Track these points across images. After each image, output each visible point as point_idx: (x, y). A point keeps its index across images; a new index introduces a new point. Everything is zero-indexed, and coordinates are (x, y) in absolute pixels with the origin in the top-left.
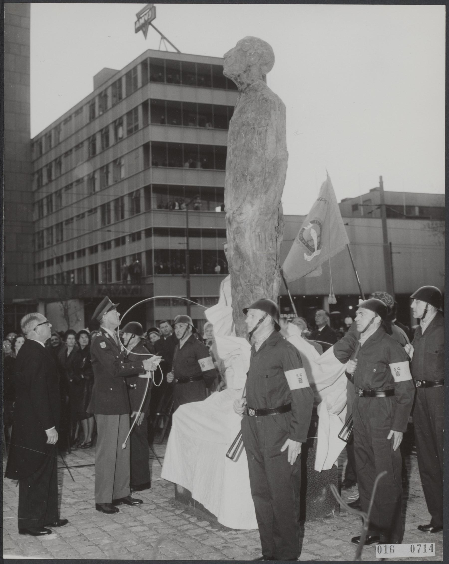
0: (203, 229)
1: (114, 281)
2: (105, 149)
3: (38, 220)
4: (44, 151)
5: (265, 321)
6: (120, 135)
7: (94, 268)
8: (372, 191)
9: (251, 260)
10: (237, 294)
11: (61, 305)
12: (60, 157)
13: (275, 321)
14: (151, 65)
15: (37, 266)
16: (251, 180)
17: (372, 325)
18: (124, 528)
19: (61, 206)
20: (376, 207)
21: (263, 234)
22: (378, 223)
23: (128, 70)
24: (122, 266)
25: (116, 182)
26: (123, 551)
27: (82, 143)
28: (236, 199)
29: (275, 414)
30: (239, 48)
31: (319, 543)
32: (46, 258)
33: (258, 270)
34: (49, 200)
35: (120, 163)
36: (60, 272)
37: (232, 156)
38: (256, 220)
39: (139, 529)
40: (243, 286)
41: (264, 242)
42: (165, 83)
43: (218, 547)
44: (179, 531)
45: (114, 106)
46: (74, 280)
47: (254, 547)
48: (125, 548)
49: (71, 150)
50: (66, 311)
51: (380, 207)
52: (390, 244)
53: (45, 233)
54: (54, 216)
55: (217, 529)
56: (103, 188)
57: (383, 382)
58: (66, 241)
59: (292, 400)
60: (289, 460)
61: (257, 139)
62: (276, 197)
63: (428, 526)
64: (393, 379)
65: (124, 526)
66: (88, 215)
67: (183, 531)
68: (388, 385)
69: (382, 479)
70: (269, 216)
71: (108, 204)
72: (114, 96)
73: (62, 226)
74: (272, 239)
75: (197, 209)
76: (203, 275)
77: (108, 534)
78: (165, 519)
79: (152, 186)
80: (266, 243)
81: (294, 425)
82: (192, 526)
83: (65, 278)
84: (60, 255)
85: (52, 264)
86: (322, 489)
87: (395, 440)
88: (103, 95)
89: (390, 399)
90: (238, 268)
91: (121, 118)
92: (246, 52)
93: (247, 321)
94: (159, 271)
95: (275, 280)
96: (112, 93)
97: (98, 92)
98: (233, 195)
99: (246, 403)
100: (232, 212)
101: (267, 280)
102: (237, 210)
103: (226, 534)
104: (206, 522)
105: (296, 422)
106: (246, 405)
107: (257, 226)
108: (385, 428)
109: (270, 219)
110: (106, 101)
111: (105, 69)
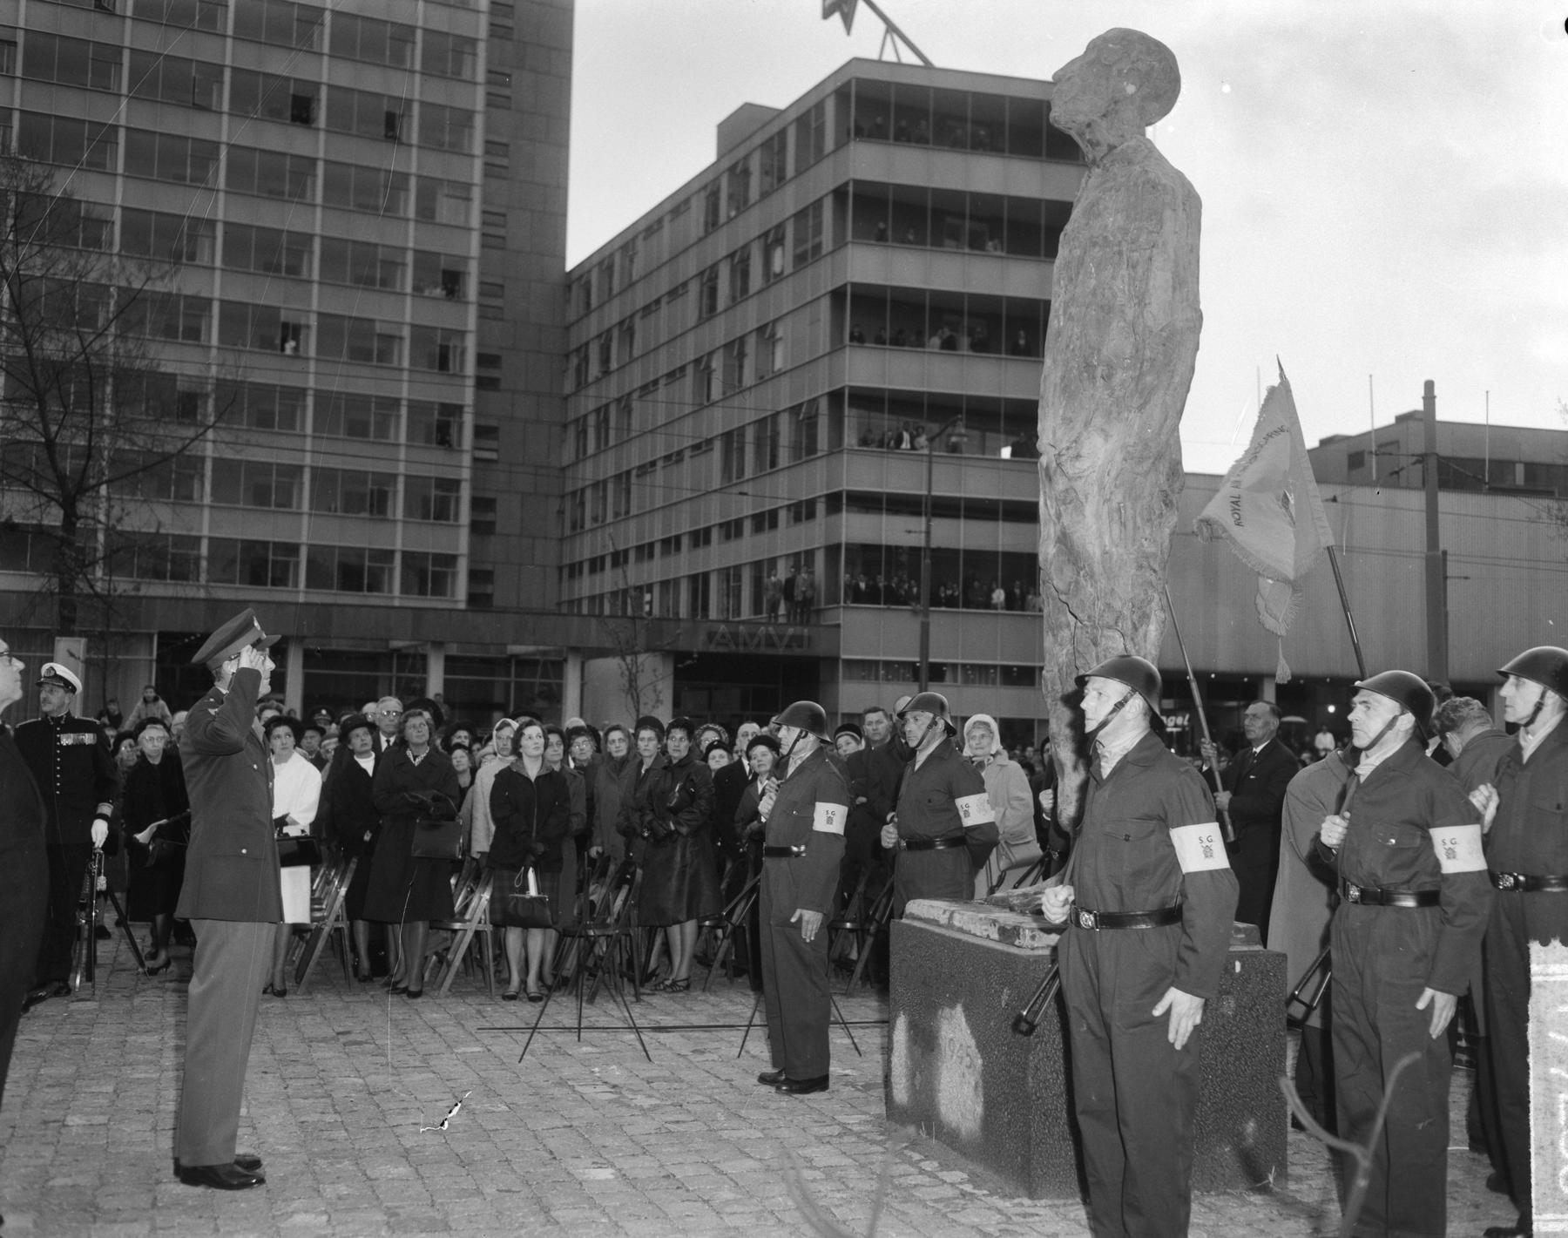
1: (746, 613)
4: (594, 303)
5: (1127, 707)
6: (777, 268)
7: (699, 583)
8: (1401, 419)
9: (1098, 569)
10: (1058, 648)
12: (632, 316)
13: (1151, 709)
14: (858, 97)
16: (1107, 378)
17: (1389, 735)
19: (629, 430)
20: (1415, 459)
21: (1128, 504)
22: (1417, 499)
23: (803, 110)
24: (766, 580)
25: (762, 380)
26: (766, 1220)
27: (685, 285)
29: (1144, 926)
30: (1093, 56)
32: (587, 555)
35: (773, 335)
38: (1113, 474)
41: (1130, 525)
42: (891, 141)
43: (991, 1230)
45: (765, 195)
46: (651, 608)
48: (772, 1212)
49: (658, 301)
50: (632, 680)
51: (1422, 459)
52: (1445, 553)
53: (588, 494)
54: (611, 455)
55: (985, 1192)
57: (1412, 871)
60: (1171, 1037)
62: (1166, 420)
64: (1437, 865)
66: (692, 457)
67: (906, 1189)
70: (1147, 465)
71: (741, 430)
72: (766, 172)
73: (628, 479)
75: (954, 449)
78: (863, 1159)
80: (1136, 528)
81: (1186, 955)
82: (926, 1180)
85: (603, 568)
87: (1437, 1012)
88: (739, 170)
91: (780, 227)
94: (857, 596)
95: (1153, 618)
96: (762, 165)
97: (726, 164)
98: (1061, 412)
99: (1072, 898)
100: (1053, 452)
101: (1134, 617)
102: (1068, 448)
103: (1008, 1204)
105: (1193, 950)
106: (1074, 902)
107: (1116, 486)
108: (1413, 982)
109: (1146, 474)
110: (747, 186)
111: (747, 107)
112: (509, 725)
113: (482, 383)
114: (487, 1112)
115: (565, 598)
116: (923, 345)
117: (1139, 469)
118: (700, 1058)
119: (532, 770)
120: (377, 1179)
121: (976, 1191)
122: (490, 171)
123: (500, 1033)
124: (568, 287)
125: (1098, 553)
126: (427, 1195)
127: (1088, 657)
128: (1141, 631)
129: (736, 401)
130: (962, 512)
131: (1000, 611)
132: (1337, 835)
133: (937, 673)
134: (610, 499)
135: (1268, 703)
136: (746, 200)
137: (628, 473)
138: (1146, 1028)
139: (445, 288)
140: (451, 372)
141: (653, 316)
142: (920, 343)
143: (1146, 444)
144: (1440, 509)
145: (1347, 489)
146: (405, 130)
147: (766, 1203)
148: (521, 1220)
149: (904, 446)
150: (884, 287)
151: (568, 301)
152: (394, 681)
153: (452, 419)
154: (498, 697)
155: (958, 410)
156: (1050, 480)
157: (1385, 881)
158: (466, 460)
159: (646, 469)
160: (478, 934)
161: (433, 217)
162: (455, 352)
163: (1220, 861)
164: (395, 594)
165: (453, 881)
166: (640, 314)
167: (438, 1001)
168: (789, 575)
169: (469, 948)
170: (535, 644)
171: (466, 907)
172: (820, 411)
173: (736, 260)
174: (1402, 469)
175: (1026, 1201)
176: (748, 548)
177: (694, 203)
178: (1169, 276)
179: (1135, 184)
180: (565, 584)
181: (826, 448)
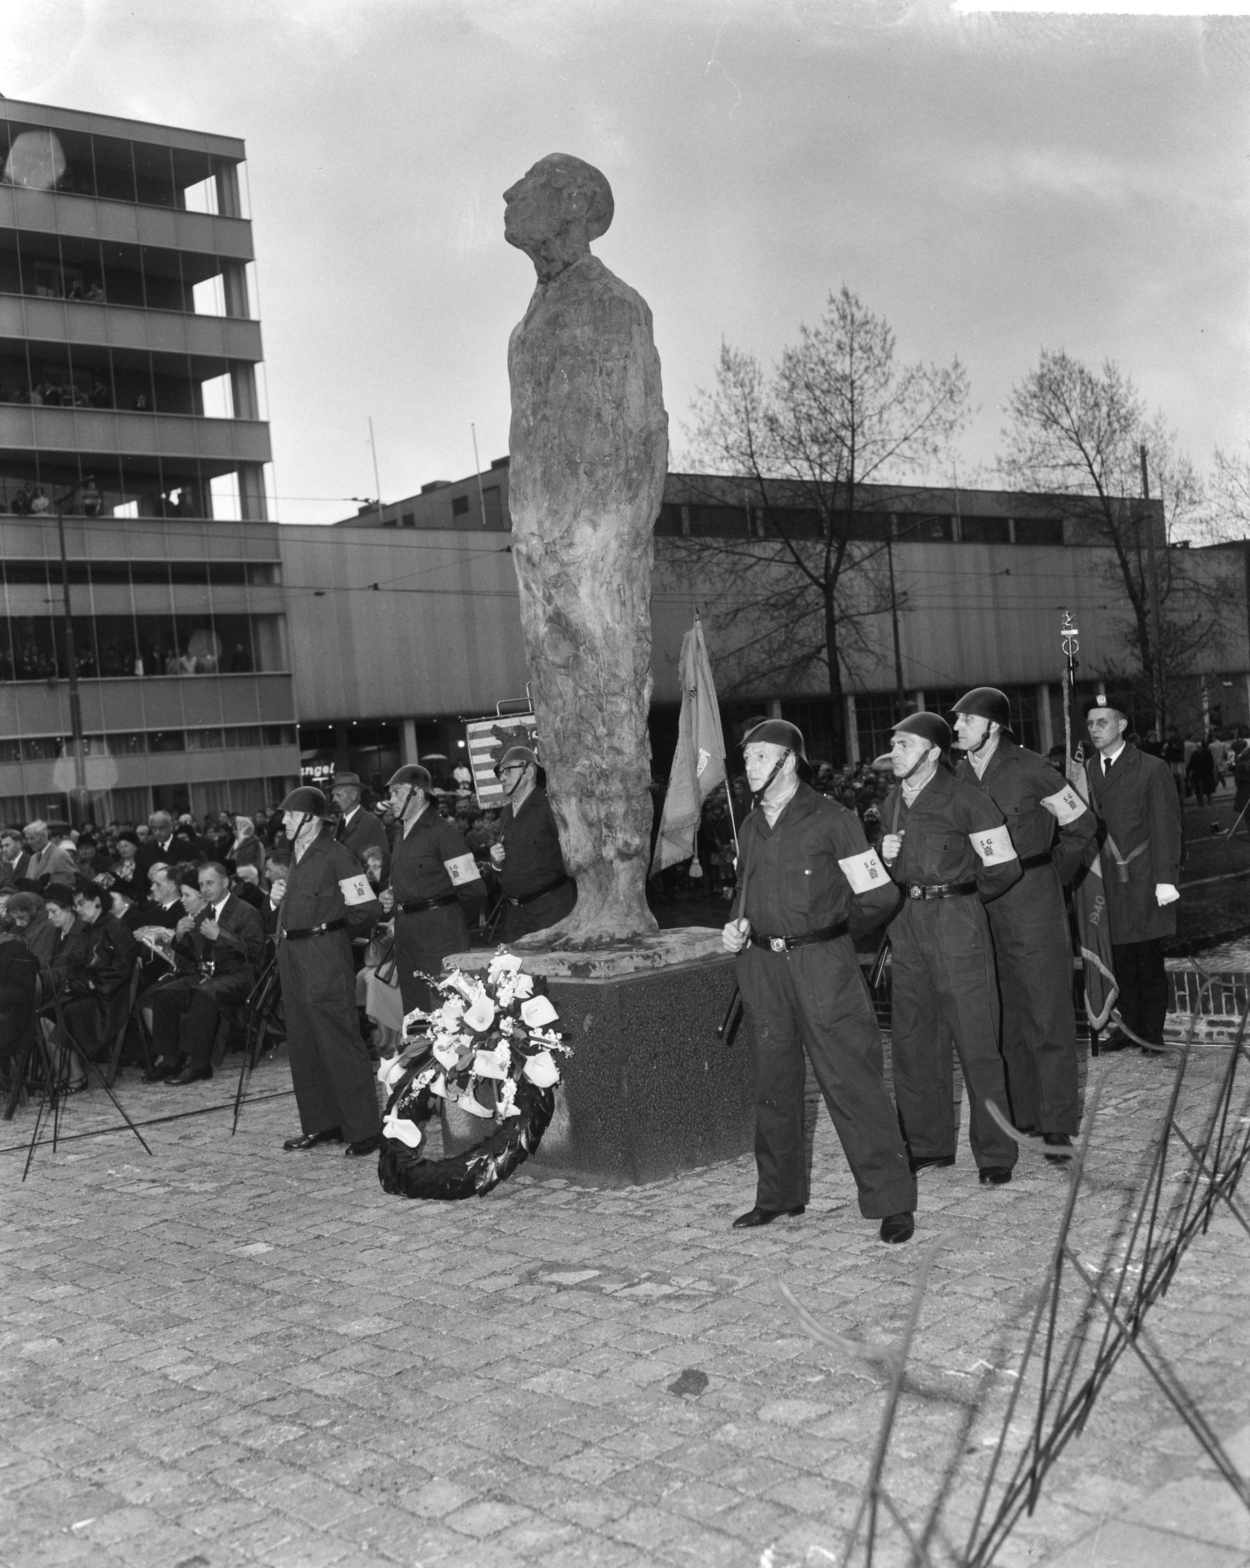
0: (93, 563)
9: (599, 643)
10: (552, 716)
33: (617, 663)
41: (629, 604)
64: (978, 859)
74: (644, 598)
76: (99, 679)
80: (633, 606)
92: (560, 190)
98: (546, 504)
109: (640, 557)
125: (599, 632)
127: (592, 721)
178: (641, 383)
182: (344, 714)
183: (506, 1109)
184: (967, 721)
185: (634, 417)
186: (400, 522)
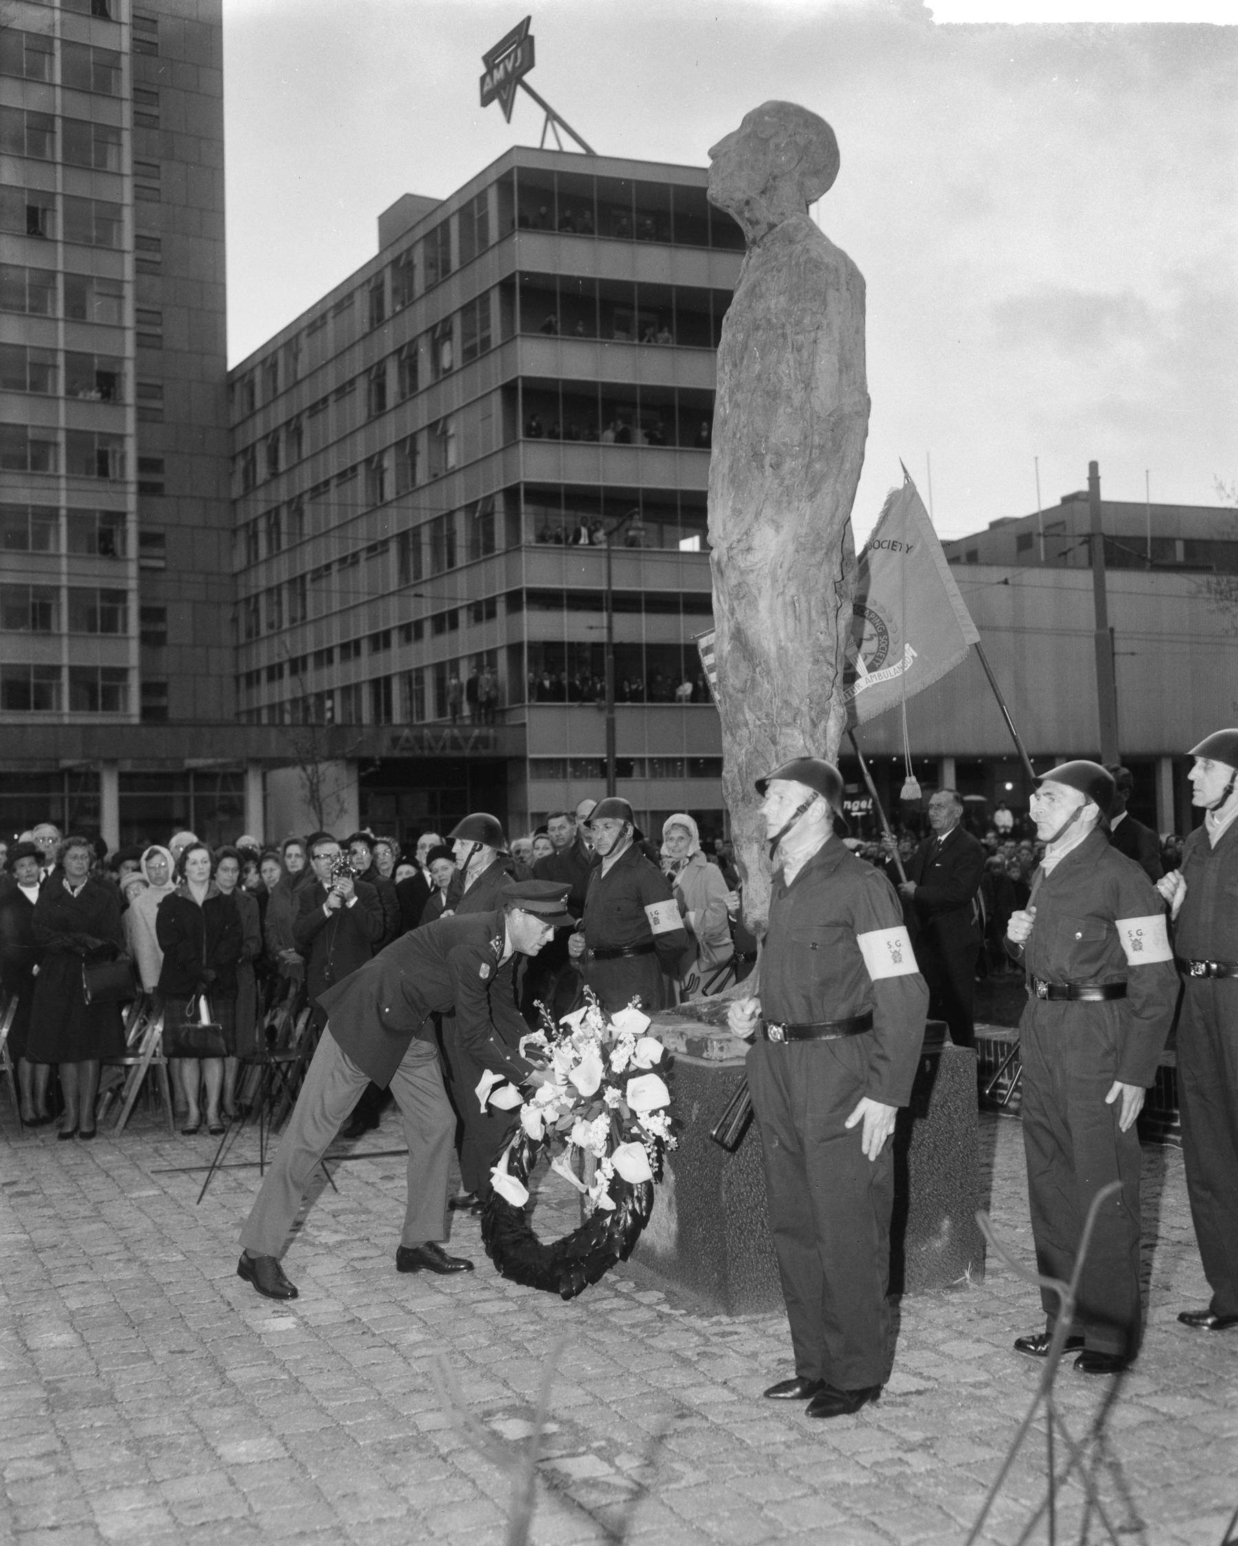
0: (648, 594)
1: (430, 716)
2: (408, 396)
3: (246, 570)
4: (258, 404)
5: (810, 810)
6: (446, 362)
7: (381, 686)
8: (1067, 500)
9: (774, 664)
10: (737, 748)
11: (303, 775)
12: (299, 416)
13: (835, 813)
15: (243, 681)
16: (776, 466)
17: (1074, 826)
18: (458, 1306)
19: (301, 535)
20: (1081, 539)
21: (803, 599)
22: (1084, 579)
25: (435, 478)
27: (352, 382)
28: (737, 512)
29: (833, 1037)
30: (748, 130)
31: (934, 1348)
32: (264, 662)
33: (789, 689)
34: (272, 520)
35: (445, 431)
36: (300, 694)
37: (727, 406)
38: (786, 566)
39: (494, 1307)
40: (751, 726)
41: (805, 619)
43: (689, 1353)
44: (593, 1314)
45: (430, 289)
47: (772, 1357)
49: (325, 400)
51: (1088, 539)
52: (1112, 630)
53: (263, 600)
54: (284, 561)
55: (683, 1312)
56: (402, 494)
58: (315, 621)
59: (875, 1004)
60: (865, 1149)
61: (791, 363)
62: (837, 507)
63: (1204, 1315)
64: (1124, 957)
65: (459, 1300)
66: (367, 559)
68: (1110, 971)
69: (1110, 1198)
71: (417, 530)
72: (430, 265)
74: (825, 613)
75: (632, 542)
76: (646, 704)
77: (420, 1319)
79: (522, 487)
80: (811, 622)
82: (621, 1303)
83: (313, 710)
84: (299, 654)
85: (281, 676)
86: (941, 1221)
87: (1125, 1105)
89: (1115, 1007)
90: (739, 685)
91: (447, 320)
92: (767, 140)
93: (765, 810)
94: (541, 695)
95: (832, 713)
96: (426, 258)
97: (389, 257)
98: (730, 503)
99: (758, 1011)
100: (725, 545)
102: (739, 541)
103: (706, 1323)
104: (655, 1293)
105: (884, 1058)
106: (761, 1015)
109: (821, 564)
111: (408, 198)
112: (157, 852)
113: (146, 489)
114: (161, 1263)
115: (243, 707)
116: (596, 438)
117: (813, 561)
118: (390, 1185)
119: (199, 894)
120: (37, 1350)
121: (673, 1312)
122: (141, 267)
123: (180, 1173)
124: (231, 387)
125: (773, 649)
126: (91, 1363)
127: (767, 756)
128: (821, 727)
129: (410, 501)
130: (643, 607)
131: (684, 704)
132: (1024, 931)
133: (624, 768)
134: (285, 607)
135: (950, 791)
136: (411, 295)
137: (303, 577)
138: (840, 1140)
139: (100, 390)
140: (111, 477)
141: (320, 416)
142: (596, 438)
143: (818, 534)
144: (1108, 587)
145: (1017, 571)
146: (48, 226)
147: (456, 1342)
148: (194, 1384)
149: (582, 541)
150: (556, 381)
151: (231, 401)
152: (67, 800)
153: (114, 527)
154: (178, 813)
155: (635, 503)
156: (722, 573)
157: (1073, 976)
158: (132, 570)
159: (321, 573)
160: (152, 1069)
161: (83, 316)
162: (114, 457)
163: (909, 965)
164: (65, 712)
165: (125, 1013)
166: (307, 414)
167: (112, 1141)
168: (471, 676)
169: (145, 1080)
170: (213, 756)
171: (139, 1040)
172: (496, 509)
173: (403, 357)
174: (1070, 550)
175: (725, 1319)
176: (430, 651)
177: (358, 297)
178: (835, 359)
179: (797, 264)
180: (243, 694)
181: (503, 546)
182: (882, 750)
183: (598, 1197)
184: (1206, 769)
185: (823, 398)
186: (964, 559)
